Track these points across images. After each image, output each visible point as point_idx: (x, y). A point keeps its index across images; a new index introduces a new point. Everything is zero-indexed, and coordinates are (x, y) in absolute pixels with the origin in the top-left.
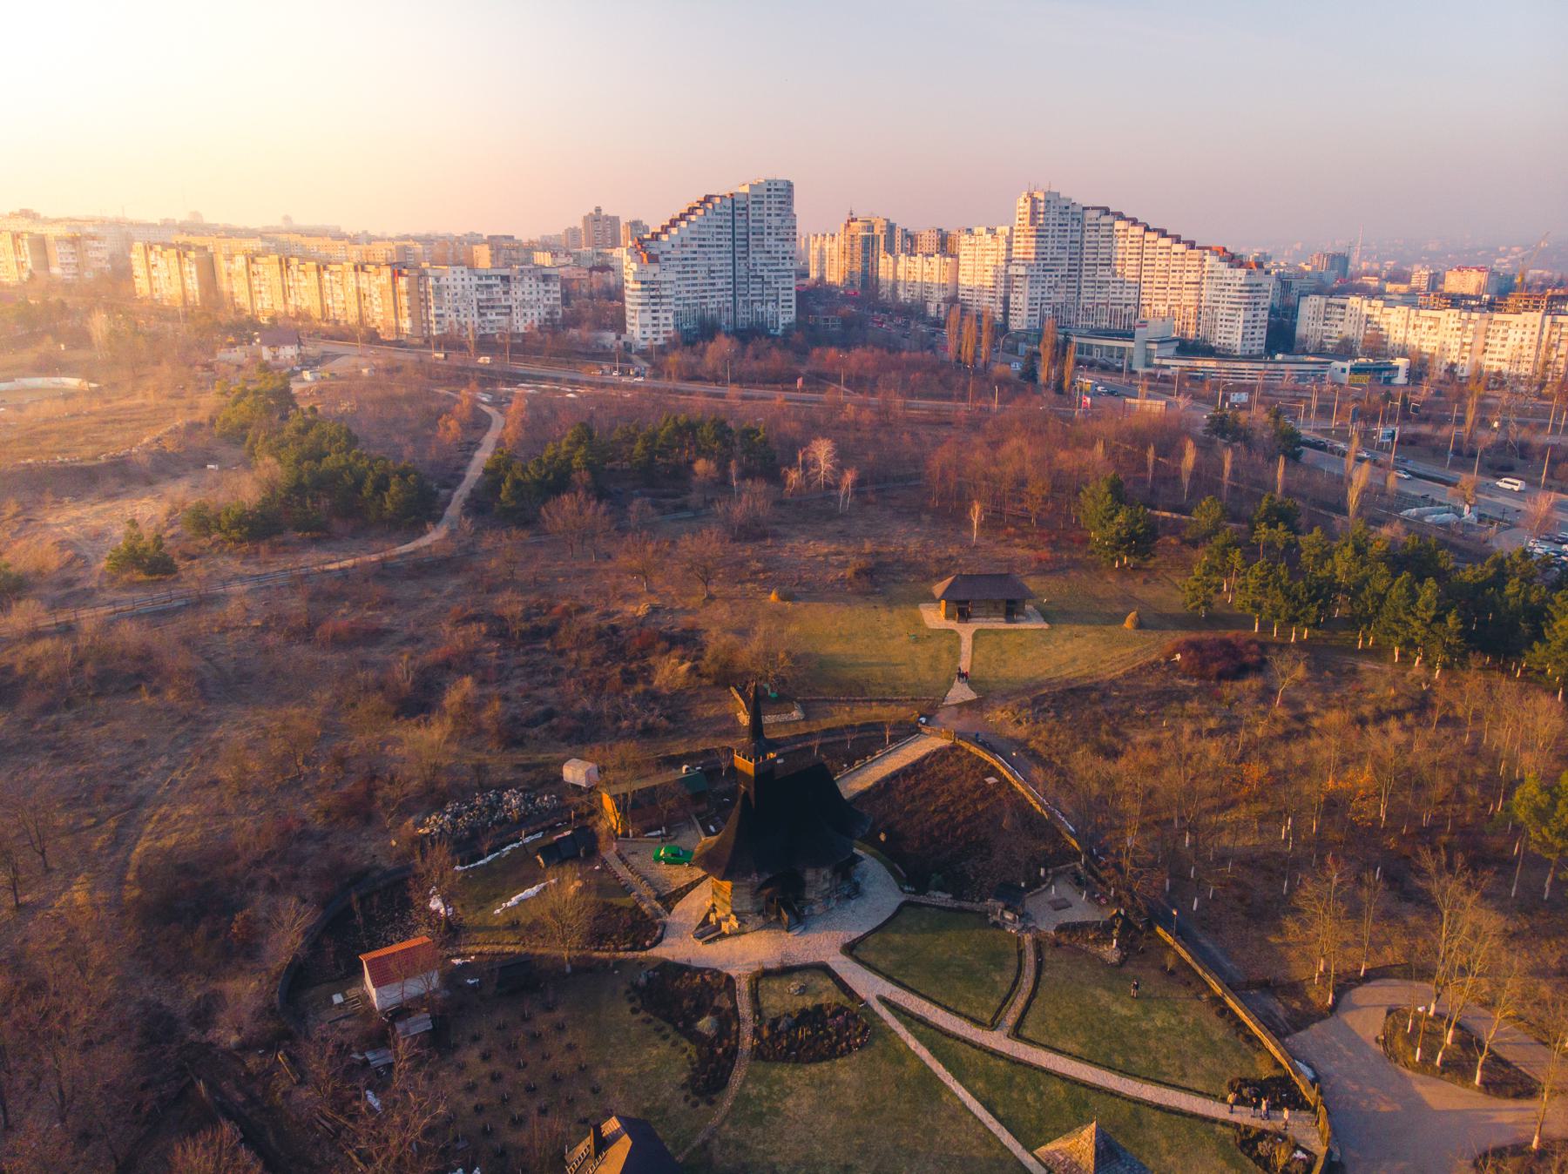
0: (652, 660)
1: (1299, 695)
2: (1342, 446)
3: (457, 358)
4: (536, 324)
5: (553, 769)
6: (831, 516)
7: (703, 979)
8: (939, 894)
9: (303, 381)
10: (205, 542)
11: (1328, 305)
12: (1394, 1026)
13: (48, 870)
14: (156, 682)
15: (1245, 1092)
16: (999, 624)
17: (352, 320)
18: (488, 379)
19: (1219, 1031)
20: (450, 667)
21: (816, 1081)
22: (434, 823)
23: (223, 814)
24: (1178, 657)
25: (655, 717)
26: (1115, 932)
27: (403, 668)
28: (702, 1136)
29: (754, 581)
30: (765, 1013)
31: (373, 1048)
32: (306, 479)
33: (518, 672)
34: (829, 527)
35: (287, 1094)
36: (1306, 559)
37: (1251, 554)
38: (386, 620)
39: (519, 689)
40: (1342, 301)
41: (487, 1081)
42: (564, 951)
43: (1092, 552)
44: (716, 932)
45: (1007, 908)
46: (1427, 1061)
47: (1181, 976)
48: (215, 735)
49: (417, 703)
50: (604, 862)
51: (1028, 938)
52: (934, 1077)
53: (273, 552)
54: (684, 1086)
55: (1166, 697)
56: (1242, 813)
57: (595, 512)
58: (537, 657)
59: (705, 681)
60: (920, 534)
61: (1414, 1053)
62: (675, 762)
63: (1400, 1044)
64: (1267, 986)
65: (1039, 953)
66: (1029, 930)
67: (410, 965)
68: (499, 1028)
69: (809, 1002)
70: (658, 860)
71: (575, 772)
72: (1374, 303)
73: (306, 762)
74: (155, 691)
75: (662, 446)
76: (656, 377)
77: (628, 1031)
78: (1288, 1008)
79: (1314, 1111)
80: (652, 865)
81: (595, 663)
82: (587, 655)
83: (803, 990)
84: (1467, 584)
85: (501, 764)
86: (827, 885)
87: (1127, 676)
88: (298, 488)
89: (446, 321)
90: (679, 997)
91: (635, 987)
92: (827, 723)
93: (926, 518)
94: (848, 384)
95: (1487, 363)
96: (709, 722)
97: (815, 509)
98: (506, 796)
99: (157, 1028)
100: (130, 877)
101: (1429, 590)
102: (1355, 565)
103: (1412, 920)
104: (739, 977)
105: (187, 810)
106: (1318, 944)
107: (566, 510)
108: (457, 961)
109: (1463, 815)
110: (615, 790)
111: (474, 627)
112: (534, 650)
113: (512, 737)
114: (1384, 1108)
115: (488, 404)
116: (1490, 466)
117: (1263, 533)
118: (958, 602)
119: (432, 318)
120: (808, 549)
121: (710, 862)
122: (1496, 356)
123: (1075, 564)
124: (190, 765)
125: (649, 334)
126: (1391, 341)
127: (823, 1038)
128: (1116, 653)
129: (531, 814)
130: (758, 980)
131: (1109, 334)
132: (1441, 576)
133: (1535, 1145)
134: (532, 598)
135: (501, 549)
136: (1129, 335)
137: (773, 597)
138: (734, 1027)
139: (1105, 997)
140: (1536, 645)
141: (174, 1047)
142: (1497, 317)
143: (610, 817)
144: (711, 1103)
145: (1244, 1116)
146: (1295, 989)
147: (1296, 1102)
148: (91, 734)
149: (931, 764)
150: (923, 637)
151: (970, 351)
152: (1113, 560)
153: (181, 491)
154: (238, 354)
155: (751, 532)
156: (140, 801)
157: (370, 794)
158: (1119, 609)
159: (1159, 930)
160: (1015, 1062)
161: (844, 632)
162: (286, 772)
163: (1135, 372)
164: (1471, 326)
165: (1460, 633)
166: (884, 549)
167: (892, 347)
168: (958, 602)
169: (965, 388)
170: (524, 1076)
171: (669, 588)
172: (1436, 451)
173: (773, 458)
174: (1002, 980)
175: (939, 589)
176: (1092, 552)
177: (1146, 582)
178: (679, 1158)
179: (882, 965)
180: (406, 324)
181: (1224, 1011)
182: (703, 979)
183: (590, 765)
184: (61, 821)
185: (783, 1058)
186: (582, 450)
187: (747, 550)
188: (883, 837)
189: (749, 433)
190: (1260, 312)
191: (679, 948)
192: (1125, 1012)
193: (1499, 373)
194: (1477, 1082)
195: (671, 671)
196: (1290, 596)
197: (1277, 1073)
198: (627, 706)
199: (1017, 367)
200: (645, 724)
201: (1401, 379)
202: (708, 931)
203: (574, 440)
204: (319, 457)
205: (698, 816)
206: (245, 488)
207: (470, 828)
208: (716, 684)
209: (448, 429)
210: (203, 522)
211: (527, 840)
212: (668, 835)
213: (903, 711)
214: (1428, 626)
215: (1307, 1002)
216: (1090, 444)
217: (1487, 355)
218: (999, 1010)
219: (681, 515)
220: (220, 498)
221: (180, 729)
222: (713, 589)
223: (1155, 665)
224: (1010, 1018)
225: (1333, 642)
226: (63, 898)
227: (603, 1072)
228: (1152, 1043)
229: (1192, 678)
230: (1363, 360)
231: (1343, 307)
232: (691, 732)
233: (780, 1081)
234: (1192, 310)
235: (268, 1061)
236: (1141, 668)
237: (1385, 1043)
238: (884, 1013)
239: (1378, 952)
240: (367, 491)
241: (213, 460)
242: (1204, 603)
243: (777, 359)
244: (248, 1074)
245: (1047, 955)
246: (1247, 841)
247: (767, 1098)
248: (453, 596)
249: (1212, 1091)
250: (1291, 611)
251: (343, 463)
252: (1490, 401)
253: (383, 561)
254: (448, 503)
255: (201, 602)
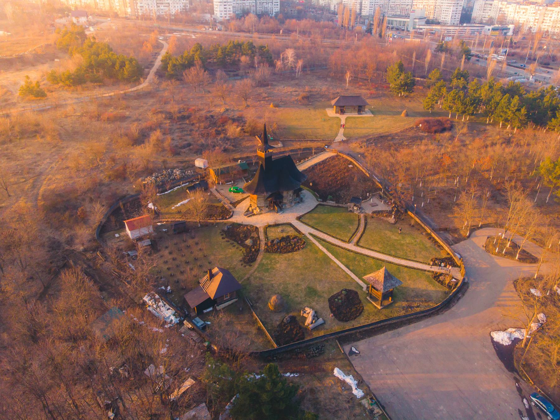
0: (226, 127)
1: (464, 138)
2: (486, 56)
3: (148, 23)
4: (179, 10)
5: (191, 163)
6: (293, 78)
7: (247, 228)
8: (331, 202)
9: (90, 31)
10: (56, 86)
11: (485, 4)
12: (489, 242)
13: (9, 196)
14: (42, 133)
15: (436, 262)
16: (355, 115)
17: (107, 8)
18: (162, 31)
19: (429, 244)
20: (151, 129)
21: (287, 259)
22: (149, 180)
23: (71, 178)
24: (421, 125)
25: (228, 146)
26: (393, 213)
27: (134, 128)
28: (247, 276)
29: (264, 101)
30: (269, 238)
31: (130, 250)
32: (93, 62)
33: (177, 130)
34: (292, 82)
35: (101, 265)
36: (471, 92)
37: (450, 89)
38: (128, 113)
39: (178, 136)
40: (491, 2)
41: (171, 260)
42: (196, 219)
43: (391, 91)
44: (251, 212)
45: (355, 205)
46: (499, 253)
47: (416, 227)
48: (67, 152)
49: (140, 139)
50: (211, 192)
51: (362, 215)
52: (328, 257)
53: (83, 90)
54: (241, 261)
55: (415, 139)
56: (441, 175)
57: (204, 75)
58: (184, 126)
59: (246, 134)
60: (327, 85)
61: (495, 250)
62: (236, 160)
63: (491, 247)
64: (446, 230)
65: (366, 220)
66: (362, 213)
67: (142, 224)
68: (175, 244)
69: (285, 235)
70: (231, 191)
71: (199, 163)
72: (503, 3)
73: (101, 160)
74: (43, 137)
75: (228, 52)
76: (226, 31)
77: (221, 244)
78: (453, 237)
79: (460, 267)
80: (226, 193)
81: (205, 128)
82: (202, 125)
83: (282, 231)
84: (530, 98)
85: (172, 161)
86: (291, 198)
87: (401, 132)
88: (91, 66)
89: (144, 9)
90: (237, 234)
91: (223, 231)
92: (291, 148)
93: (329, 79)
94: (300, 32)
95: (543, 27)
96: (248, 148)
97: (288, 75)
98: (175, 171)
99: (54, 246)
100: (40, 198)
101: (516, 100)
102: (489, 92)
103: (499, 209)
104: (260, 227)
105: (58, 177)
106: (465, 216)
107: (192, 74)
108: (159, 224)
109: (520, 177)
110: (214, 168)
111: (160, 115)
112: (183, 124)
113: (176, 152)
114: (484, 266)
115: (162, 40)
116: (541, 63)
117: (455, 82)
118: (340, 107)
119: (138, 8)
120: (284, 90)
121: (249, 189)
122: (547, 24)
123: (384, 95)
124: (58, 162)
125: (223, 15)
126: (508, 19)
127: (289, 246)
128: (398, 124)
129: (184, 177)
130: (266, 228)
131: (399, 16)
132: (520, 95)
133: (535, 277)
134: (181, 106)
135: (168, 88)
136: (407, 16)
137: (271, 106)
138: (258, 243)
139: (388, 233)
140: (553, 119)
141: (61, 251)
142: (549, 8)
143: (213, 177)
144: (250, 266)
145: (436, 269)
146: (456, 230)
147: (454, 265)
148: (20, 151)
149: (329, 161)
150: (327, 119)
151: (347, 22)
152: (398, 93)
153: (46, 68)
154: (63, 21)
155: (262, 83)
156: (41, 174)
157: (125, 170)
158: (400, 110)
159: (409, 213)
160: (357, 253)
161: (298, 118)
162: (93, 164)
163: (408, 31)
164: (539, 12)
165: (526, 115)
166: (313, 90)
167: (317, 19)
168: (340, 107)
169: (344, 35)
170: (184, 259)
171: (232, 103)
172: (522, 58)
173: (271, 58)
174: (353, 228)
175: (333, 102)
176: (391, 91)
177: (410, 101)
178: (240, 283)
179: (310, 223)
180: (129, 10)
181: (431, 238)
182: (247, 228)
183: (205, 160)
184: (12, 180)
185: (276, 252)
186: (198, 53)
187: (261, 90)
188: (311, 184)
189: (262, 48)
190: (459, 7)
191: (239, 218)
192: (396, 238)
193: (547, 31)
194: (517, 258)
195: (233, 130)
196: (464, 104)
197: (448, 256)
198: (218, 142)
199: (364, 28)
200: (224, 148)
201: (510, 33)
202: (249, 213)
203: (195, 50)
204: (98, 55)
205: (244, 178)
206: (70, 65)
207: (162, 181)
208: (250, 135)
209: (147, 47)
210: (54, 78)
211: (183, 185)
212: (234, 184)
213: (319, 144)
214: (514, 113)
215: (460, 235)
216: (392, 51)
217: (544, 24)
218: (351, 237)
219: (236, 78)
220: (61, 70)
221: (53, 150)
222: (249, 103)
223: (412, 128)
224: (355, 239)
225: (478, 121)
226: (16, 205)
227: (213, 257)
228: (405, 248)
229: (425, 132)
230: (497, 26)
231: (491, 5)
232: (241, 151)
233: (274, 259)
234: (432, 7)
235: (94, 255)
236: (407, 129)
237: (486, 247)
238: (311, 238)
239: (486, 219)
240: (117, 67)
241: (58, 58)
242: (431, 107)
243: (272, 24)
244: (88, 259)
245: (369, 220)
246: (442, 185)
247: (270, 264)
248: (152, 105)
249: (425, 262)
250: (463, 109)
251: (107, 56)
252: (543, 42)
253: (125, 93)
254: (148, 74)
255: (56, 107)
